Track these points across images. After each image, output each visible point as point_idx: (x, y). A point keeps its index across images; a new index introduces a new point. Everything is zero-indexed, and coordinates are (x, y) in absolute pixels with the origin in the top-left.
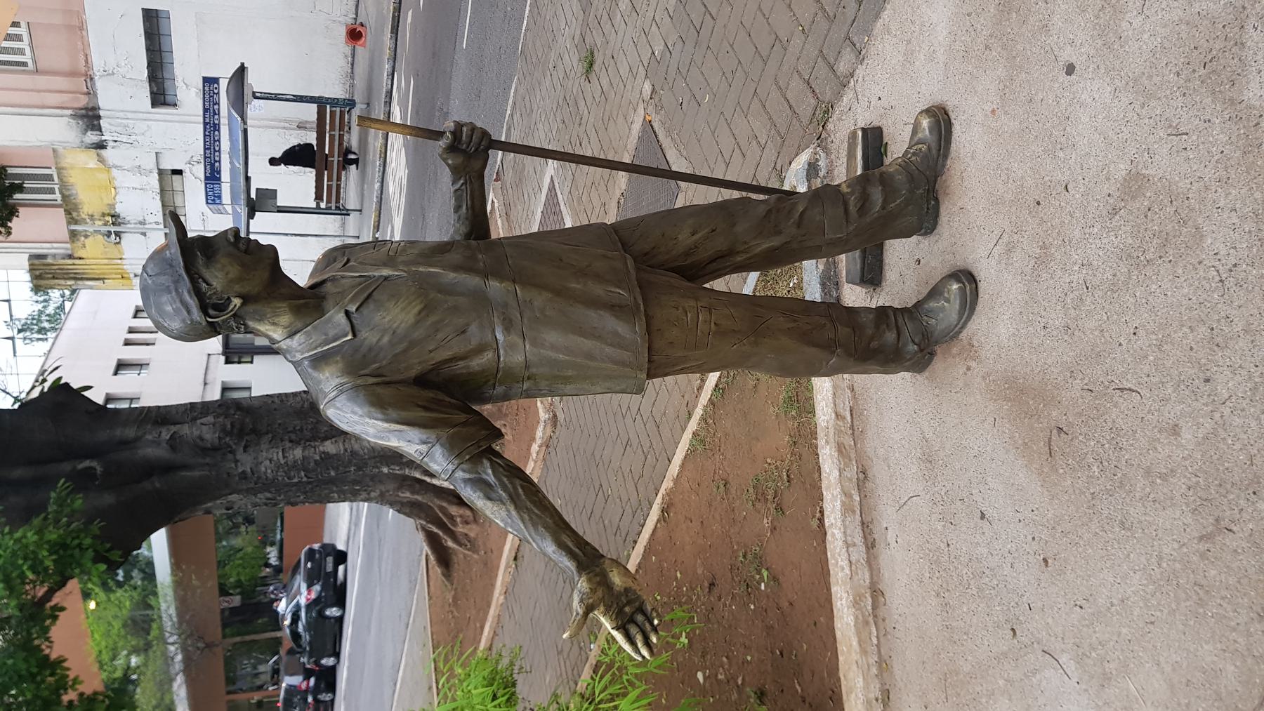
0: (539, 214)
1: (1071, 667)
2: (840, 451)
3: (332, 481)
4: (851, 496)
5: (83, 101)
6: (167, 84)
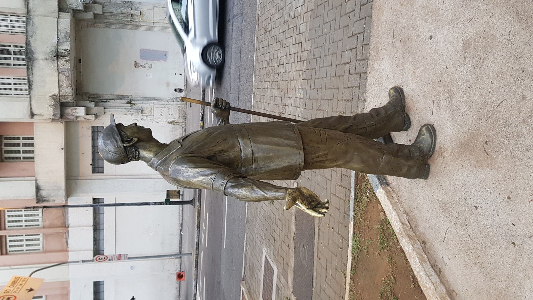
0: (263, 276)
4: (422, 255)
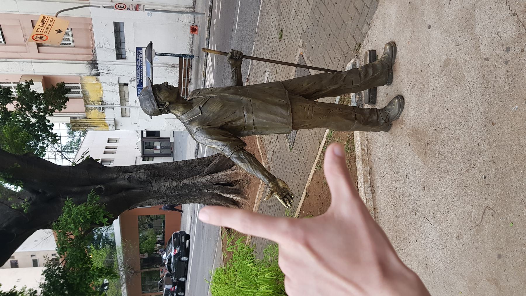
1: (431, 220)
2: (363, 161)
3: (187, 195)
5: (91, 58)
6: (123, 50)
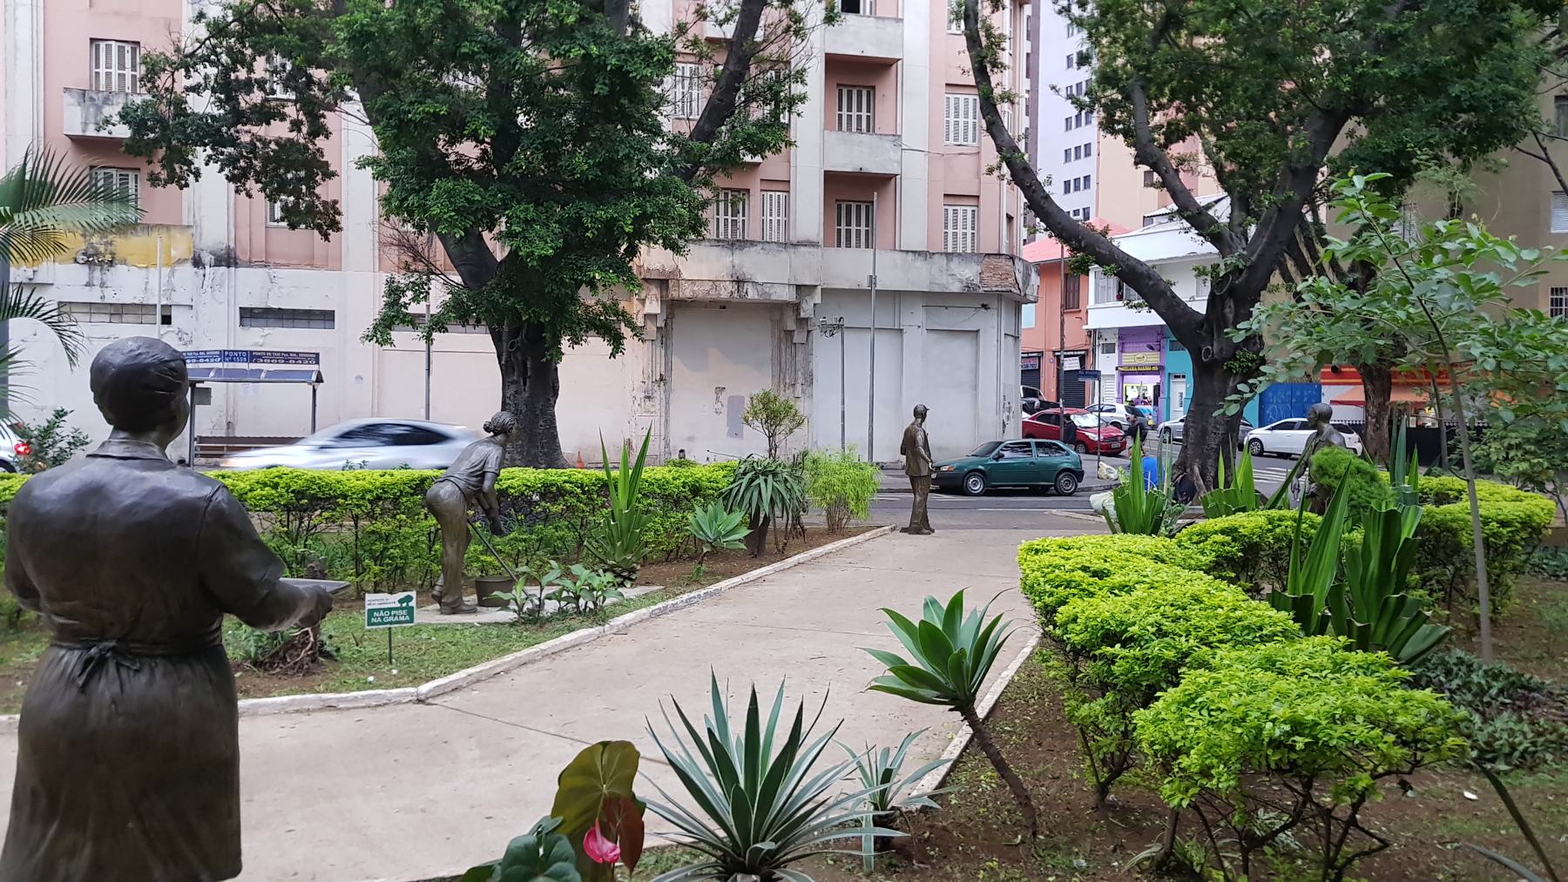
6: (262, 321)
